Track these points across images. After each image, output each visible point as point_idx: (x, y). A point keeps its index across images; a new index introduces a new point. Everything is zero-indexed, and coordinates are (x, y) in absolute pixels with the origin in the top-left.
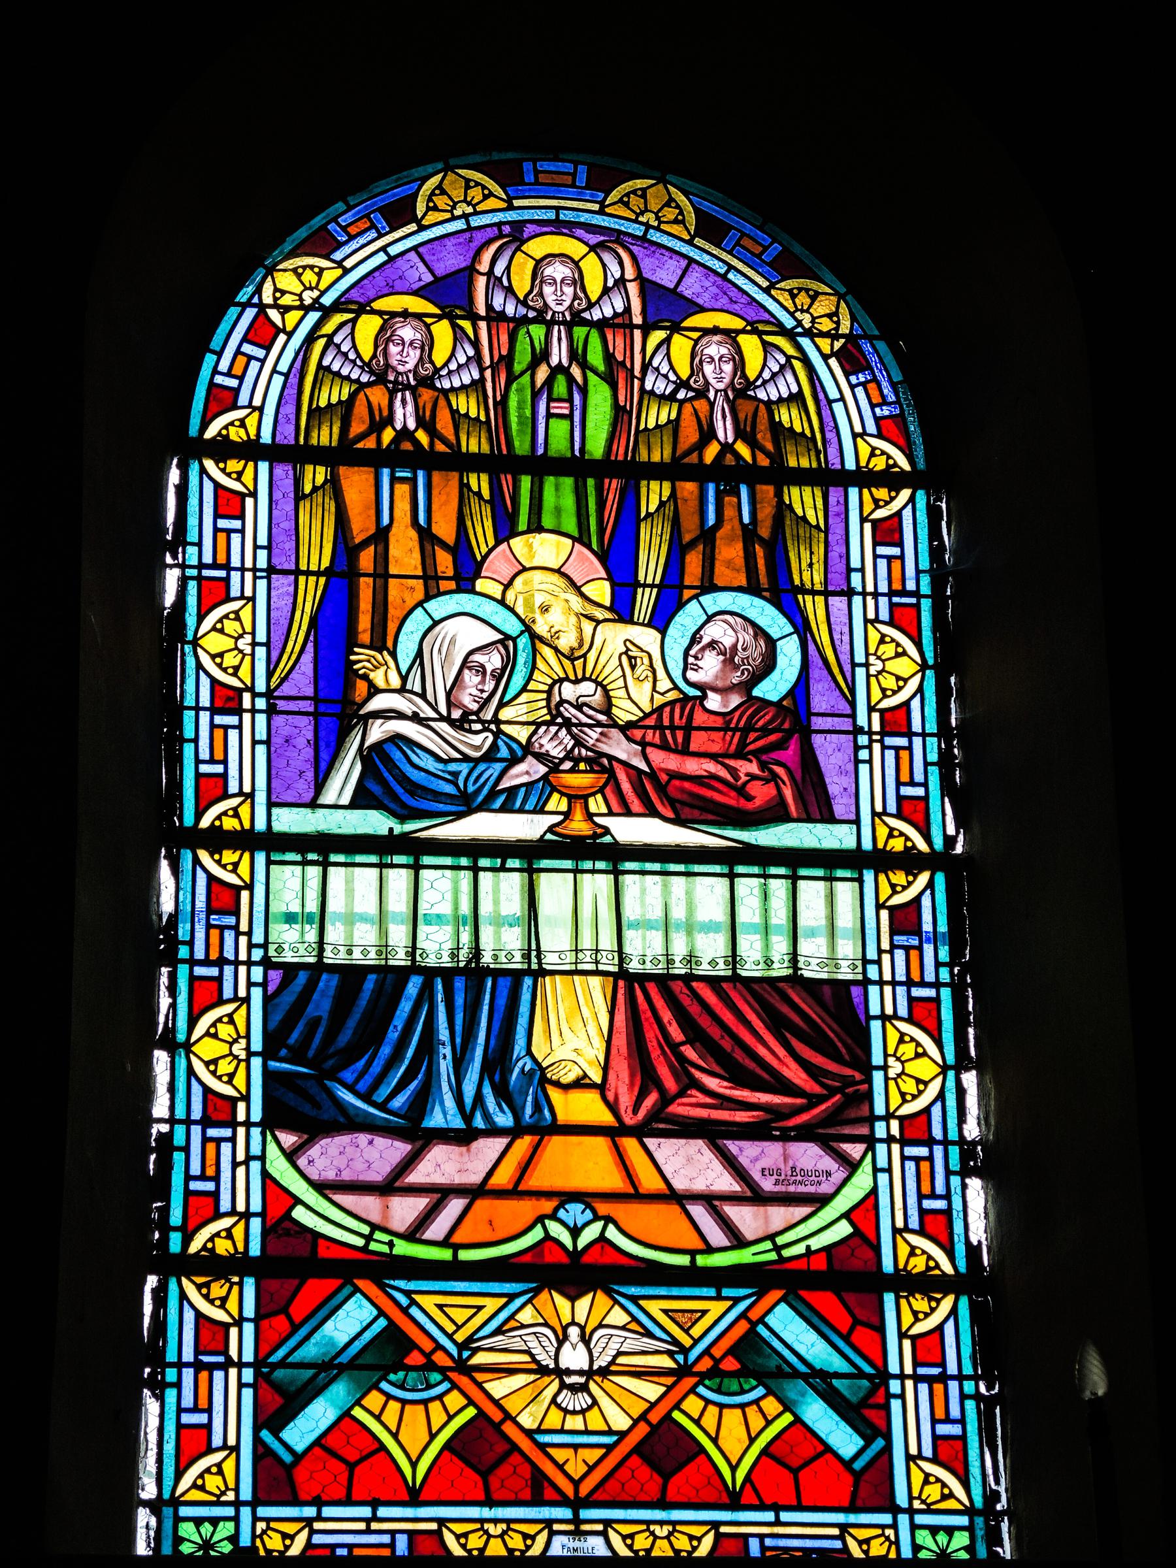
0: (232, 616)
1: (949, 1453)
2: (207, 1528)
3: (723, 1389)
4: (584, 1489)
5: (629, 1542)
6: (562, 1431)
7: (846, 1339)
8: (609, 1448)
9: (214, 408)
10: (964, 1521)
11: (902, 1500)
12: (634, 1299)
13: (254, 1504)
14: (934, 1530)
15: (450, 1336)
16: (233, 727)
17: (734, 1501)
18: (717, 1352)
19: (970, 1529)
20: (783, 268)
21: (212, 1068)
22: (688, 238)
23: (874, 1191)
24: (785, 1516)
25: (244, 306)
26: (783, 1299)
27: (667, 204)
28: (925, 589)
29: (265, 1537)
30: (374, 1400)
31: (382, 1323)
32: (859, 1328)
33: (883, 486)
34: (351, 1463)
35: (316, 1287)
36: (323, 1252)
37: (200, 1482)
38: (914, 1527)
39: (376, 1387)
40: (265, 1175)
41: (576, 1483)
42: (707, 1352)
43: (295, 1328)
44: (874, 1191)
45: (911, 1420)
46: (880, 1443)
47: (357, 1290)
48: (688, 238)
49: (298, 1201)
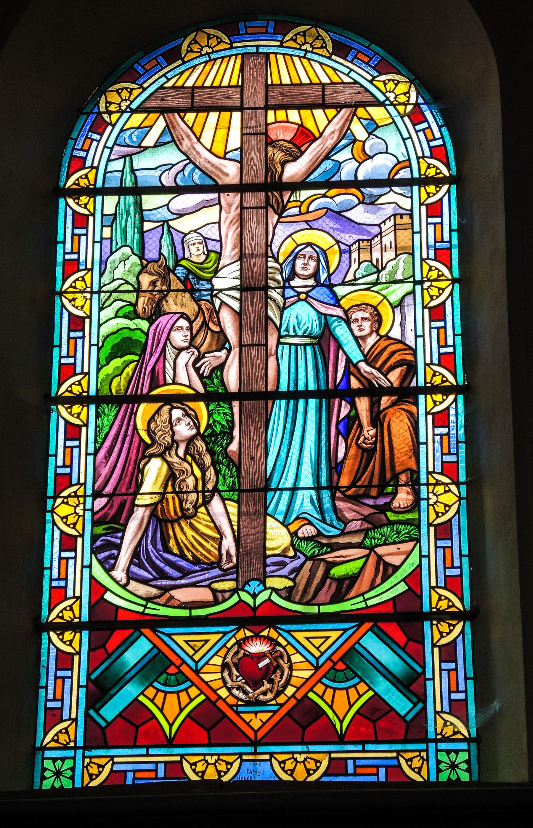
0: (80, 279)
1: (457, 708)
2: (59, 763)
3: (336, 679)
4: (260, 735)
5: (282, 765)
6: (298, 652)
7: (403, 649)
8: (275, 712)
9: (72, 170)
10: (464, 746)
11: (431, 736)
12: (289, 632)
13: (85, 748)
14: (448, 752)
15: (191, 657)
16: (80, 338)
17: (341, 740)
18: (335, 658)
19: (468, 750)
20: (382, 68)
21: (65, 520)
22: (328, 55)
23: (420, 565)
24: (368, 747)
25: (89, 114)
26: (371, 629)
27: (317, 38)
28: (455, 241)
29: (89, 767)
30: (151, 692)
31: (155, 651)
32: (411, 644)
33: (439, 393)
34: (137, 727)
35: (118, 636)
36: (121, 617)
37: (56, 738)
38: (437, 751)
39: (151, 685)
40: (92, 577)
41: (256, 732)
42: (329, 658)
43: (109, 656)
44: (420, 565)
45: (437, 694)
46: (420, 705)
47: (142, 634)
48: (328, 55)
49: (107, 589)
